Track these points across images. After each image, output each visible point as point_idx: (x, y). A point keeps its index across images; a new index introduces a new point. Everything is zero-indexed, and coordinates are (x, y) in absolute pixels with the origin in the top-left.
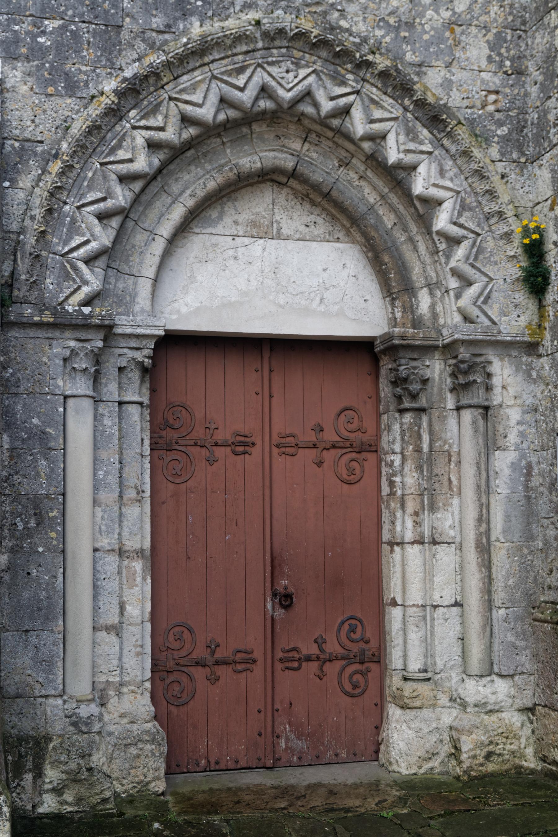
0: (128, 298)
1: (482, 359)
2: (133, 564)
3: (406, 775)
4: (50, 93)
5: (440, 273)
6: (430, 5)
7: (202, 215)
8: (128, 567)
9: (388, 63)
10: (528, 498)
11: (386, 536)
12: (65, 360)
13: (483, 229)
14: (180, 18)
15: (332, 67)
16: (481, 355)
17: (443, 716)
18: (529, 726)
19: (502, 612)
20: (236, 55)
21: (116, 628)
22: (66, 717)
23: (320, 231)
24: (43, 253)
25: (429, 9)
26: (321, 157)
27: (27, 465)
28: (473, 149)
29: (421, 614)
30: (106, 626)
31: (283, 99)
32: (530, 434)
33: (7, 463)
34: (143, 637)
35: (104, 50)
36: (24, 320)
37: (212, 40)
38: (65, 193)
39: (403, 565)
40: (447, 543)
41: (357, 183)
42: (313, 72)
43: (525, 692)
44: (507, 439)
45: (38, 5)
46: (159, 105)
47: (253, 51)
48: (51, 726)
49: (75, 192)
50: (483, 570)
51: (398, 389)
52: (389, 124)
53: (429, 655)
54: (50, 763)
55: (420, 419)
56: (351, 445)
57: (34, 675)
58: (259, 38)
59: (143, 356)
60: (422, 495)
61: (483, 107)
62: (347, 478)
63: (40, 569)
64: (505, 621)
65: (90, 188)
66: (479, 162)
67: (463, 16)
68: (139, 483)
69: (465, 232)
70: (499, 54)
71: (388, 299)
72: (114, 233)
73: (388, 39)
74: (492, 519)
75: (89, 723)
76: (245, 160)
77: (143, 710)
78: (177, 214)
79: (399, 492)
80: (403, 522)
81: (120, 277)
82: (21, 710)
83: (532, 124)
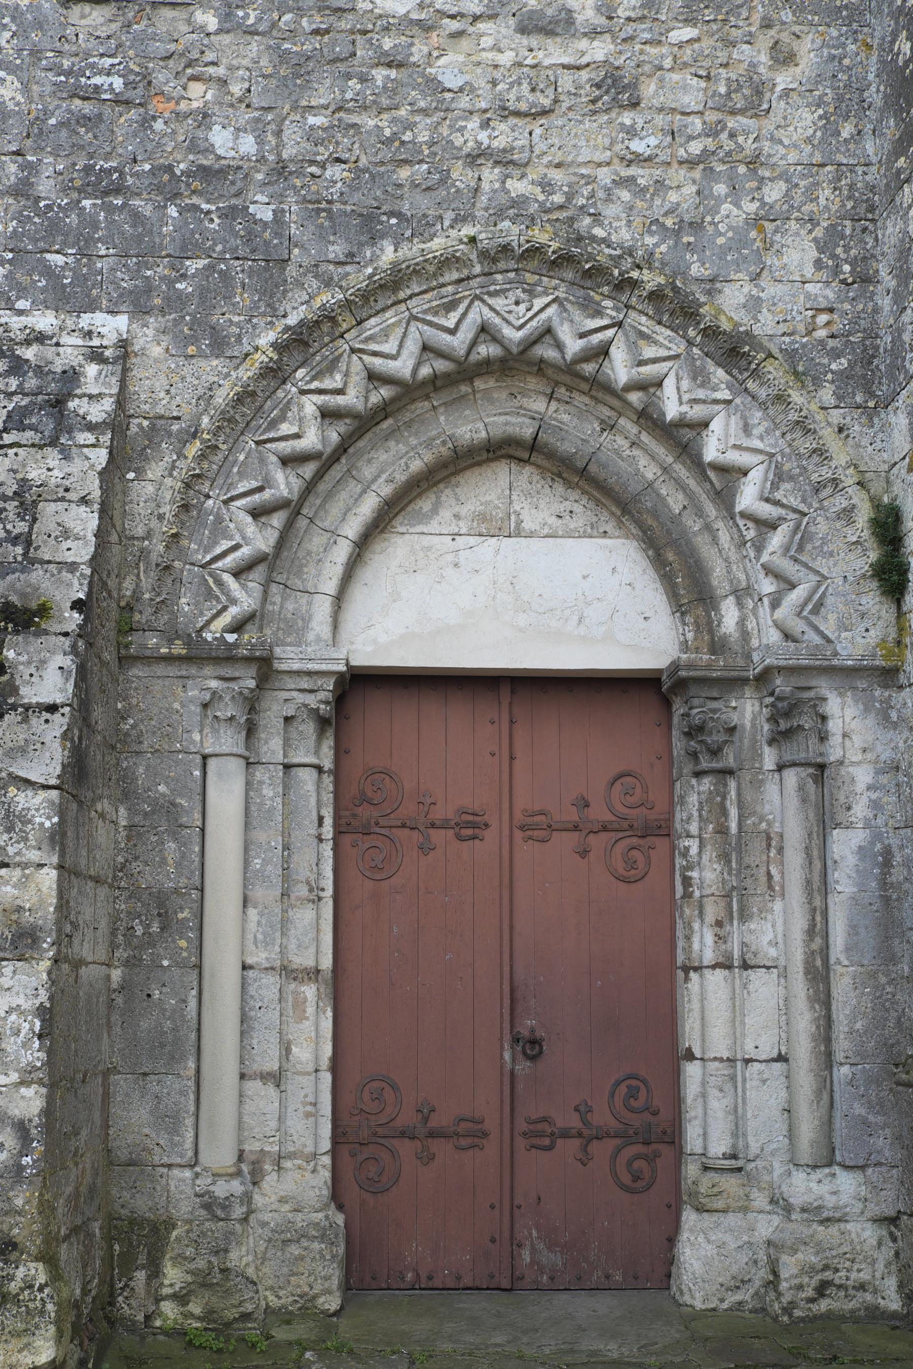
0: (300, 623)
1: (812, 694)
2: (303, 989)
3: (701, 1310)
4: (191, 353)
5: (751, 573)
6: (727, 196)
7: (409, 509)
8: (296, 993)
9: (661, 280)
10: (886, 900)
11: (680, 959)
12: (205, 706)
13: (810, 506)
14: (367, 242)
15: (581, 293)
16: (810, 688)
17: (759, 1225)
18: (891, 1245)
19: (845, 1070)
20: (443, 285)
21: (274, 1077)
22: (197, 1195)
23: (577, 523)
24: (177, 564)
25: (726, 202)
26: (576, 419)
27: (150, 848)
28: (790, 391)
29: (726, 1072)
30: (261, 1073)
31: (510, 340)
32: (888, 803)
33: (123, 845)
34: (316, 1092)
35: (263, 293)
36: (148, 653)
37: (408, 267)
38: (207, 484)
39: (702, 1000)
40: (764, 967)
41: (628, 452)
42: (554, 301)
43: (882, 1193)
44: (852, 812)
45: (177, 241)
46: (337, 359)
47: (468, 278)
48: (174, 1208)
49: (221, 482)
50: (817, 1006)
51: (692, 743)
52: (663, 367)
53: (740, 1133)
54: (171, 1258)
55: (725, 785)
56: (631, 827)
57: (153, 1135)
58: (476, 260)
59: (320, 699)
60: (728, 896)
61: (809, 333)
62: (625, 874)
63: (164, 990)
64: (850, 1083)
65: (242, 475)
66: (801, 410)
67: (777, 207)
68: (313, 877)
69: (782, 512)
70: (834, 256)
71: (678, 614)
72: (276, 534)
73: (663, 248)
74: (831, 931)
75: (227, 1207)
76: (464, 429)
77: (312, 1193)
78: (368, 507)
79: (697, 894)
80: (702, 937)
81: (290, 596)
82: (135, 1182)
83: (885, 351)
